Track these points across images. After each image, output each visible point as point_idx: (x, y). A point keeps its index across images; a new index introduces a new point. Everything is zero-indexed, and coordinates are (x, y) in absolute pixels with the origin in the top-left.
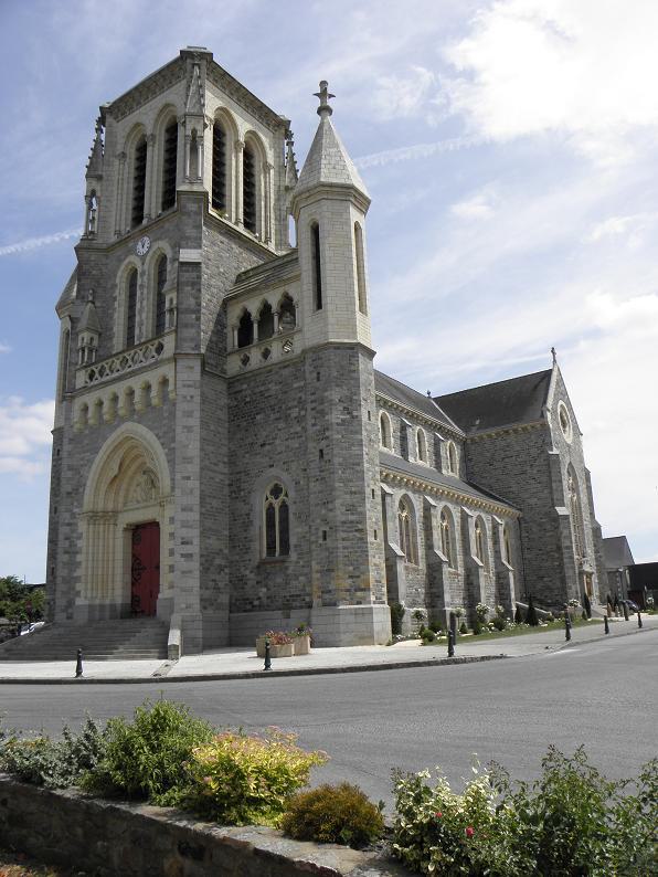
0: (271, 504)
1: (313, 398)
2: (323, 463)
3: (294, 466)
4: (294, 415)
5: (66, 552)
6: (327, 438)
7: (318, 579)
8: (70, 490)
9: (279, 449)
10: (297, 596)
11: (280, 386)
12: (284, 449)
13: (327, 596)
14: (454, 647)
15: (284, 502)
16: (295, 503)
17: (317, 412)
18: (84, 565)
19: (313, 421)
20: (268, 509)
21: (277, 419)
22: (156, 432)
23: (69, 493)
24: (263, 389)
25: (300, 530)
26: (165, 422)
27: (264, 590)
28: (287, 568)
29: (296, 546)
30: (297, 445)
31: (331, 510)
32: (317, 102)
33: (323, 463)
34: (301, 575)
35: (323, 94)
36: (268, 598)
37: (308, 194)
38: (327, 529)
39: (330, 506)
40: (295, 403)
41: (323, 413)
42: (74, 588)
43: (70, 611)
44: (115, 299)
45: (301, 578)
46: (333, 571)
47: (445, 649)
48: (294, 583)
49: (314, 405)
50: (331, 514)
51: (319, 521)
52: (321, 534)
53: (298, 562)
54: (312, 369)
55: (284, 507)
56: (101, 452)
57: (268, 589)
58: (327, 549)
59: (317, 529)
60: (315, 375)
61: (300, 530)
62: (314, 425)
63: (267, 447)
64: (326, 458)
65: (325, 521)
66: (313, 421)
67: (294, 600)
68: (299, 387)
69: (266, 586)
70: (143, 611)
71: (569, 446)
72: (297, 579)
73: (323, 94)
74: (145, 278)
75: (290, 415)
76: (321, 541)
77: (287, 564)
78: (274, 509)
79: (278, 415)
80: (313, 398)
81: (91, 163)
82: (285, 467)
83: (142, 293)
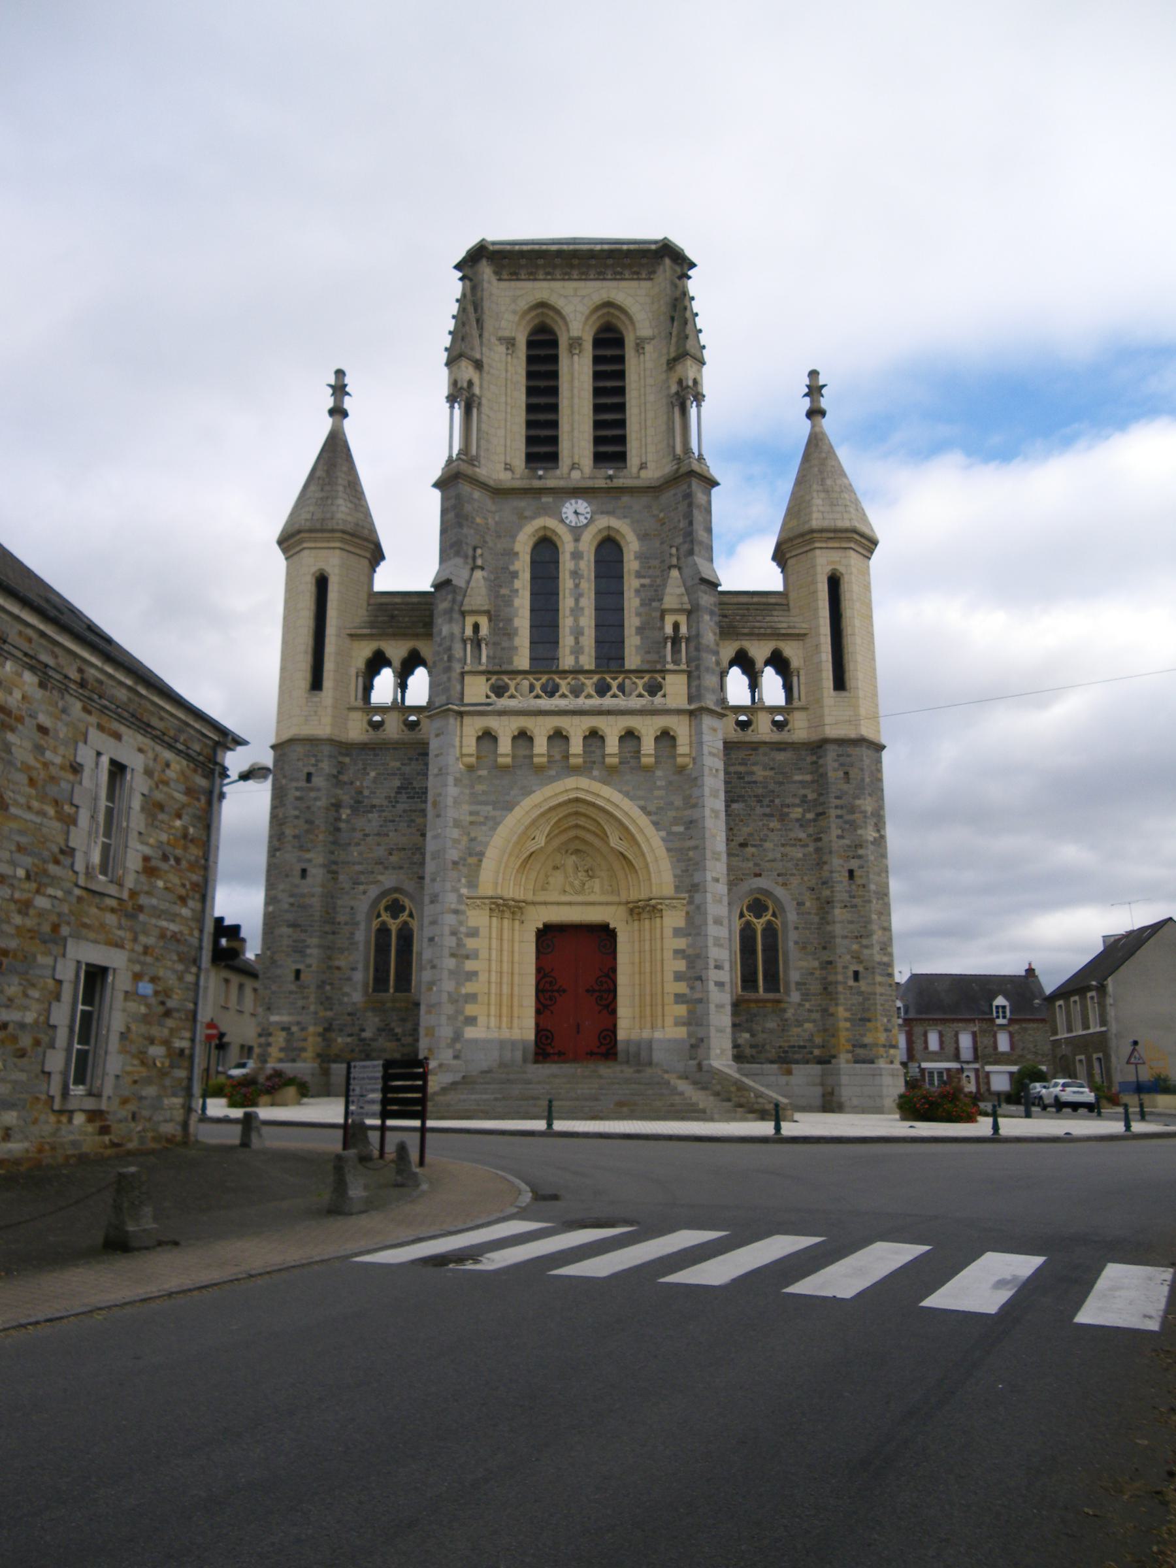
0: (748, 923)
1: (838, 802)
2: (854, 887)
3: (795, 881)
4: (793, 816)
5: (453, 955)
6: (860, 857)
7: (847, 1030)
8: (456, 859)
9: (770, 856)
10: (800, 1047)
11: (771, 773)
12: (779, 856)
13: (859, 1051)
14: (783, 1124)
15: (769, 923)
16: (796, 928)
17: (846, 822)
18: (483, 977)
19: (839, 832)
20: (742, 931)
21: (765, 815)
22: (642, 803)
23: (455, 863)
24: (741, 769)
25: (804, 964)
26: (657, 793)
27: (747, 1035)
28: (784, 1010)
29: (798, 984)
30: (800, 855)
31: (866, 947)
32: (806, 403)
33: (854, 887)
34: (808, 1021)
35: (814, 390)
36: (752, 1046)
37: (832, 535)
38: (860, 969)
39: (865, 942)
40: (797, 801)
41: (854, 826)
42: (462, 1012)
43: (458, 1046)
44: (515, 575)
45: (808, 1026)
46: (869, 1020)
47: (772, 1124)
48: (795, 1030)
49: (839, 812)
50: (866, 952)
51: (848, 957)
52: (851, 974)
53: (800, 1005)
54: (836, 765)
55: (770, 931)
56: (518, 812)
57: (753, 1035)
58: (861, 993)
59: (845, 967)
60: (841, 774)
61: (804, 964)
62: (840, 837)
63: (750, 850)
64: (860, 881)
65: (857, 958)
66: (839, 832)
67: (795, 1053)
68: (801, 782)
69: (750, 1031)
70: (560, 1054)
71: (378, 774)
72: (802, 1025)
73: (814, 390)
74: (583, 564)
75: (787, 814)
76: (851, 983)
77: (783, 1005)
78: (754, 931)
79: (768, 810)
80: (838, 802)
81: (453, 341)
82: (780, 879)
83: (577, 586)
